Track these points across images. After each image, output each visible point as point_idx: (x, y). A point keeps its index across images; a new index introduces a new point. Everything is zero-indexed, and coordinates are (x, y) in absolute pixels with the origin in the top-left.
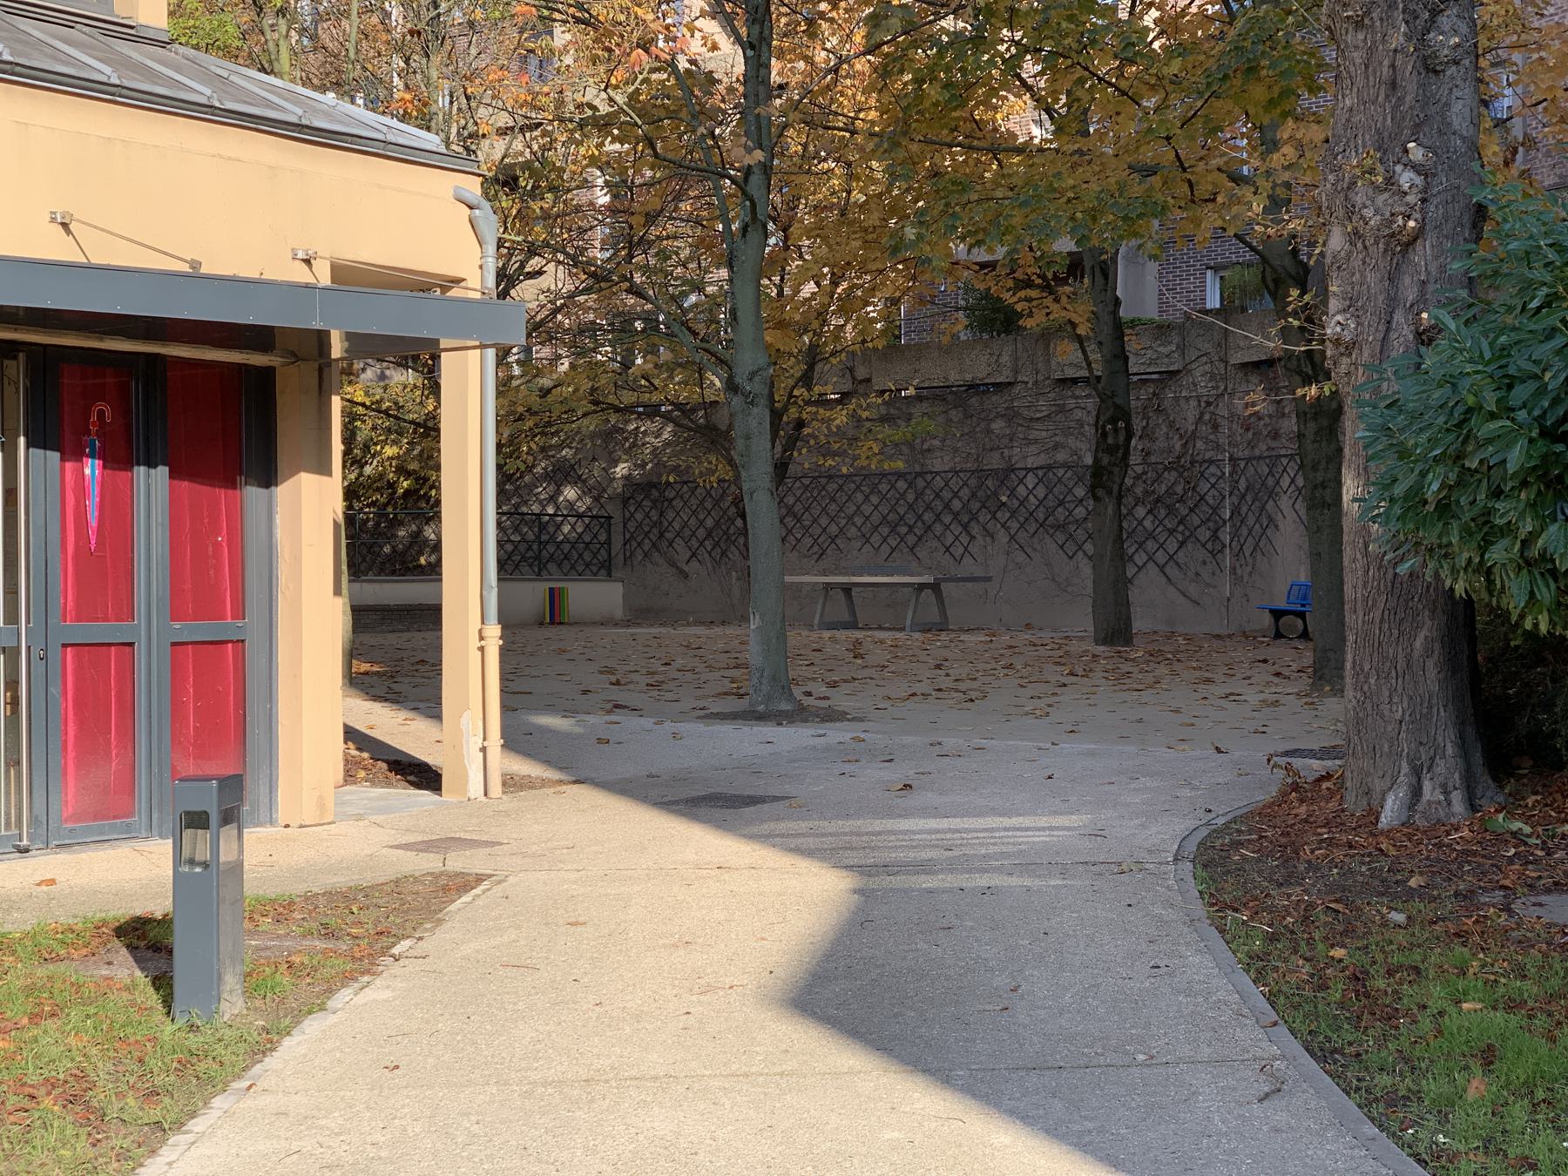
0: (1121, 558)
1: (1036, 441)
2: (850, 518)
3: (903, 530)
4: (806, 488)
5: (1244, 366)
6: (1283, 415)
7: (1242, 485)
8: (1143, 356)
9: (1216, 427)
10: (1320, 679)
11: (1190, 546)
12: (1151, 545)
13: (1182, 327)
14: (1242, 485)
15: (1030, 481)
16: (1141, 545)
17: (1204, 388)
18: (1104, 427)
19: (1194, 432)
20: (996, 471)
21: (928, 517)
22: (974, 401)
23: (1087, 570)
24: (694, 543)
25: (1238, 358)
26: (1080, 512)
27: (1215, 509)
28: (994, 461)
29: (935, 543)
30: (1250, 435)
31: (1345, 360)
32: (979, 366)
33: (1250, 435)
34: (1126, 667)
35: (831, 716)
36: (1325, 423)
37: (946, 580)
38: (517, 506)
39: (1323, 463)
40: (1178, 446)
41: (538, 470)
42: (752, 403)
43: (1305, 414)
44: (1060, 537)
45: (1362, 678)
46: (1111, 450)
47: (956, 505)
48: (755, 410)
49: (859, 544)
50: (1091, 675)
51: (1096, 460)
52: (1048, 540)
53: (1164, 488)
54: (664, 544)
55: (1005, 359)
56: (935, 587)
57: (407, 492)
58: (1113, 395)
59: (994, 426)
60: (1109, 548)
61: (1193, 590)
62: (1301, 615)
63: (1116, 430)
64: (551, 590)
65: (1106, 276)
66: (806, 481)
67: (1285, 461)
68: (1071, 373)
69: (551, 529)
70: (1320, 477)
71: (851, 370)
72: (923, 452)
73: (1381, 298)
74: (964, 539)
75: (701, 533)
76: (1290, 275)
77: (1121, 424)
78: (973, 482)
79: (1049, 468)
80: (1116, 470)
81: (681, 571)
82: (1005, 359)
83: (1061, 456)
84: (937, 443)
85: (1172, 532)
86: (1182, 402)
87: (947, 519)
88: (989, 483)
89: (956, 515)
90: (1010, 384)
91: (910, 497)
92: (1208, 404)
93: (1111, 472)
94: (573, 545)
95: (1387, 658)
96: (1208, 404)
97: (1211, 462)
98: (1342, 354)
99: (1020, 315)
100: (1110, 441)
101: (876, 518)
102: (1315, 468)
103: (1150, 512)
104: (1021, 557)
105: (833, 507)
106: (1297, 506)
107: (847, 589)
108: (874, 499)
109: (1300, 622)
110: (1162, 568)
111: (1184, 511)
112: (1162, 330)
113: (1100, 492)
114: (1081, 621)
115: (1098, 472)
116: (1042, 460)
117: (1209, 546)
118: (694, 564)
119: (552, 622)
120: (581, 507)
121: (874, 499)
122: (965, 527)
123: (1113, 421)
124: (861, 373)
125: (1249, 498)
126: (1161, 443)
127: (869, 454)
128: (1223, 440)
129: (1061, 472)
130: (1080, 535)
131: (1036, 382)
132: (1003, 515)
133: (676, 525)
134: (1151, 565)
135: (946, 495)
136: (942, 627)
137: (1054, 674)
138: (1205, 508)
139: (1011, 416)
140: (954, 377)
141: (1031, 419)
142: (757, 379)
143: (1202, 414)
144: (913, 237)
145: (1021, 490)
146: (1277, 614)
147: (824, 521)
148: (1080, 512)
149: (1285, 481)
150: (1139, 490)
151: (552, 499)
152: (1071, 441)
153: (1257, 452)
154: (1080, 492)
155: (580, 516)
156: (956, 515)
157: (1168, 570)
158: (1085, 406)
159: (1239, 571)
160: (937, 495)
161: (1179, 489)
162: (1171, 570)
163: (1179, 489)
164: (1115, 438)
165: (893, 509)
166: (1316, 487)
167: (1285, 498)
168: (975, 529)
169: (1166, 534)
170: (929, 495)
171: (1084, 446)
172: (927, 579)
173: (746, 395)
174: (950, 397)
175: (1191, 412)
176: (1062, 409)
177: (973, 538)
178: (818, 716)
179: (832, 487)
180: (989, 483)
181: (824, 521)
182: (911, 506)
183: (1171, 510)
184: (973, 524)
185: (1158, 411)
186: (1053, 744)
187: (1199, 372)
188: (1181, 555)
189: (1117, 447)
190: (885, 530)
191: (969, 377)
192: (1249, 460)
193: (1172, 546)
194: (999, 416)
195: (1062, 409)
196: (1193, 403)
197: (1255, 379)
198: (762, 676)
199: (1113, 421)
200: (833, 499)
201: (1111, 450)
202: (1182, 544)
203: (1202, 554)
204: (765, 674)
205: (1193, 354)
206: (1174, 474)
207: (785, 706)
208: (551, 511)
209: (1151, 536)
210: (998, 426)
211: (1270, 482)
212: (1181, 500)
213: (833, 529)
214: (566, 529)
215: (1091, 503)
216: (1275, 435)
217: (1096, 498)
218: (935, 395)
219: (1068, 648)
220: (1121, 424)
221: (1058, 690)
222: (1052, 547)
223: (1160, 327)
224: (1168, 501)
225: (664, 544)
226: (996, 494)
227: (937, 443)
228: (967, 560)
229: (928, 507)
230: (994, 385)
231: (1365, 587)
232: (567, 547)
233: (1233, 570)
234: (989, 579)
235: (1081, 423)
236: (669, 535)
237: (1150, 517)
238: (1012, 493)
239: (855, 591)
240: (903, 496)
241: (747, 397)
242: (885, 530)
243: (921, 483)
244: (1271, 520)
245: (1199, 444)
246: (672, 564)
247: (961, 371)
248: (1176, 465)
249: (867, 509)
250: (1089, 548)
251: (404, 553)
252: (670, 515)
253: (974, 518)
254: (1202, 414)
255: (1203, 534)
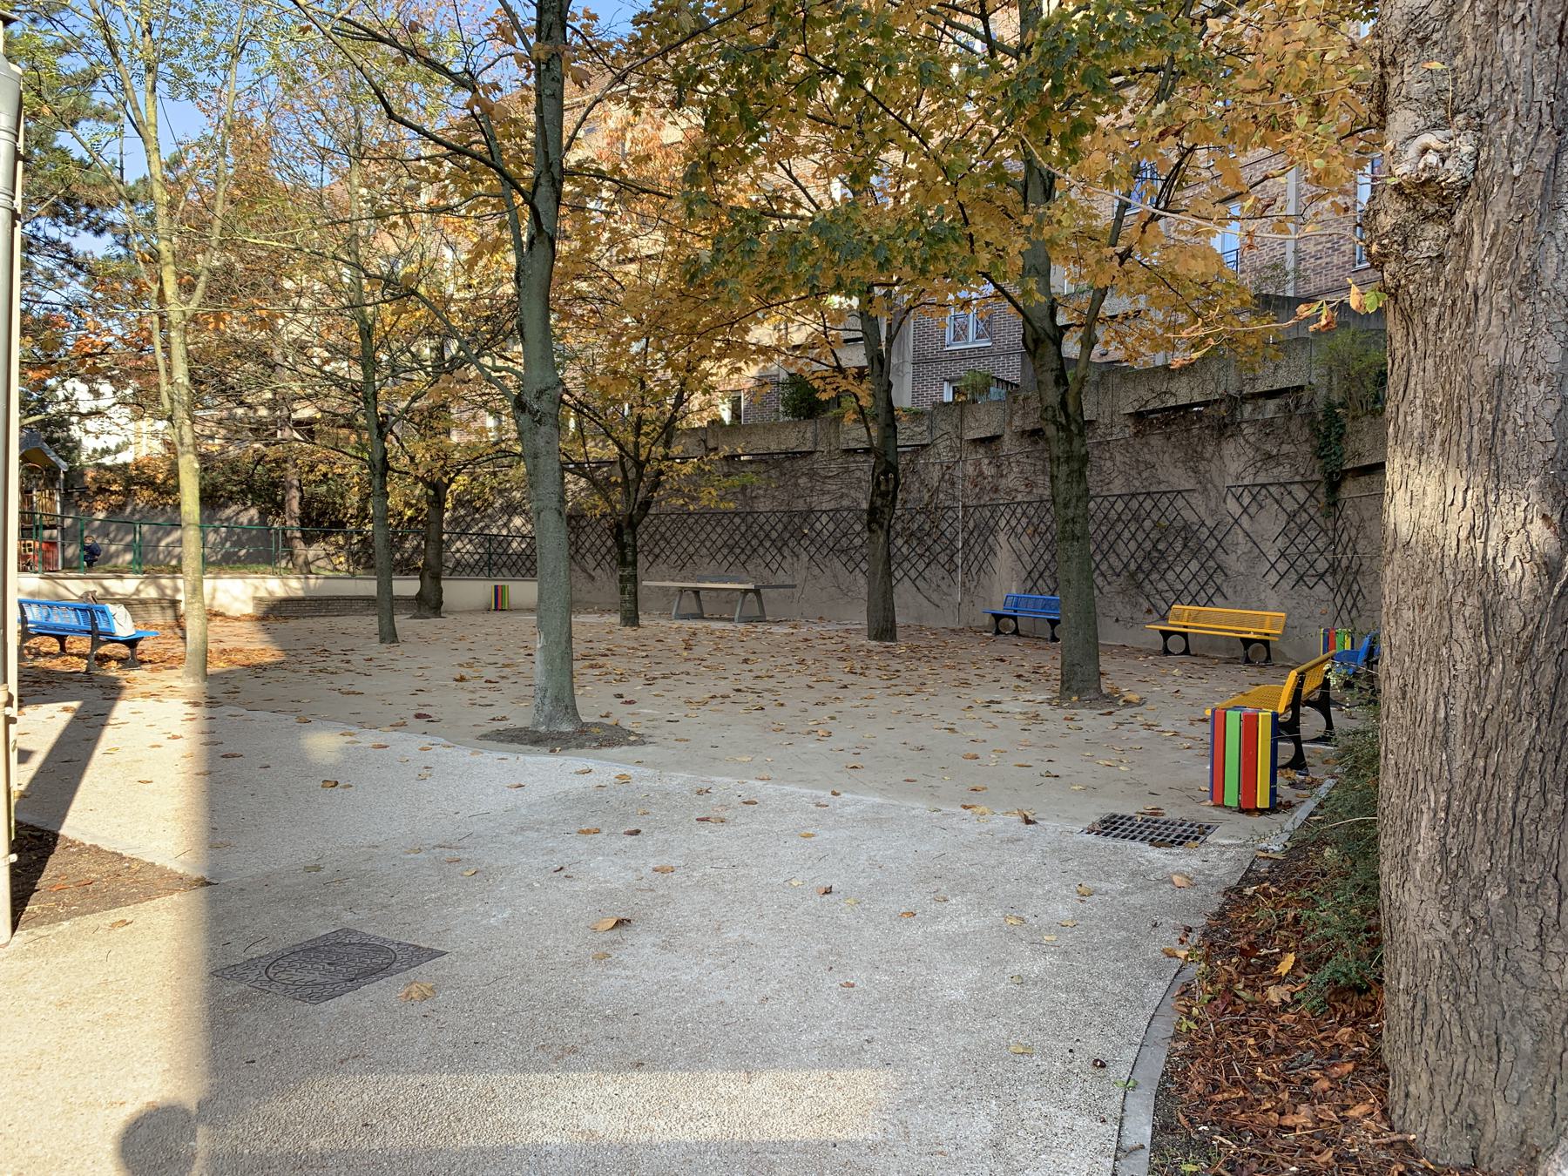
0: (889, 574)
1: (829, 492)
2: (702, 542)
3: (738, 551)
4: (673, 521)
5: (974, 441)
6: (1002, 476)
7: (971, 525)
8: (907, 434)
9: (953, 484)
10: (1068, 689)
11: (933, 566)
12: (906, 565)
13: (931, 414)
14: (971, 525)
15: (824, 519)
16: (899, 565)
17: (946, 457)
18: (878, 477)
19: (938, 487)
20: (801, 512)
21: (755, 542)
22: (787, 464)
23: (862, 581)
24: (599, 557)
25: (971, 435)
26: (858, 542)
27: (951, 542)
28: (800, 505)
29: (760, 561)
30: (977, 490)
31: (1432, 231)
32: (792, 439)
33: (977, 490)
34: (895, 664)
35: (611, 737)
36: (1076, 466)
37: (765, 587)
38: (482, 529)
39: (1074, 501)
40: (926, 497)
41: (497, 505)
42: (539, 421)
43: (1059, 458)
44: (844, 559)
45: (1464, 885)
46: (884, 495)
47: (774, 535)
48: (543, 429)
49: (708, 560)
50: (867, 672)
51: (872, 503)
52: (836, 560)
53: (916, 526)
54: (579, 557)
55: (808, 435)
56: (757, 591)
57: (411, 519)
58: (885, 454)
59: (800, 481)
60: (880, 567)
61: (935, 597)
62: (1015, 618)
63: (887, 480)
64: (496, 587)
65: (882, 365)
66: (674, 517)
67: (1002, 508)
68: (853, 445)
69: (505, 545)
70: (1070, 513)
71: (705, 441)
72: (752, 498)
73: (1541, 82)
74: (779, 558)
75: (604, 550)
76: (1049, 337)
77: (891, 476)
78: (785, 519)
79: (837, 510)
80: (886, 510)
81: (590, 576)
82: (808, 435)
83: (845, 503)
84: (761, 492)
85: (921, 556)
86: (930, 466)
87: (767, 544)
88: (796, 520)
89: (773, 541)
90: (811, 453)
91: (743, 529)
92: (948, 468)
93: (883, 512)
94: (519, 556)
95: (1533, 852)
96: (948, 468)
97: (949, 508)
98: (1427, 218)
99: (817, 391)
100: (883, 488)
101: (719, 543)
102: (1066, 506)
103: (906, 542)
104: (817, 571)
105: (691, 534)
106: (1011, 540)
107: (696, 592)
108: (719, 530)
109: (1011, 622)
110: (914, 582)
111: (930, 542)
112: (917, 416)
113: (874, 526)
114: (858, 618)
115: (872, 511)
116: (832, 505)
117: (947, 566)
118: (599, 571)
119: (496, 609)
120: (525, 531)
121: (719, 530)
122: (780, 550)
123: (885, 473)
124: (711, 444)
125: (975, 534)
126: (915, 495)
127: (709, 497)
128: (958, 493)
129: (845, 514)
130: (858, 557)
131: (829, 452)
132: (804, 542)
133: (587, 544)
134: (906, 578)
135: (767, 528)
136: (761, 619)
137: (838, 671)
138: (944, 540)
139: (812, 475)
140: (774, 447)
141: (826, 477)
142: (545, 397)
143: (943, 475)
144: (708, 261)
145: (818, 526)
146: (998, 617)
147: (685, 544)
148: (858, 542)
149: (1003, 523)
150: (898, 527)
151: (506, 525)
152: (852, 492)
153: (982, 502)
154: (858, 527)
155: (524, 537)
156: (773, 541)
157: (917, 582)
158: (864, 468)
159: (967, 584)
160: (761, 528)
161: (927, 527)
162: (920, 583)
163: (927, 527)
164: (887, 485)
165: (731, 536)
166: (1067, 522)
167: (1002, 534)
168: (786, 552)
169: (916, 558)
170: (756, 528)
171: (861, 496)
172: (751, 586)
173: (534, 413)
174: (771, 462)
175: (936, 473)
176: (847, 470)
177: (784, 557)
178: (596, 740)
179: (690, 521)
180: (796, 520)
181: (685, 544)
182: (743, 535)
183: (920, 541)
184: (785, 548)
185: (914, 472)
186: (834, 794)
187: (942, 445)
188: (927, 574)
189: (888, 493)
190: (725, 551)
191: (783, 447)
192: (976, 507)
193: (921, 566)
194: (803, 474)
195: (847, 470)
196: (938, 467)
197: (982, 451)
198: (544, 697)
199: (885, 473)
200: (691, 529)
201: (884, 495)
202: (928, 565)
203: (942, 572)
204: (548, 694)
205: (938, 433)
206: (923, 516)
207: (566, 728)
208: (504, 532)
209: (906, 558)
210: (802, 481)
211: (992, 523)
212: (928, 534)
213: (691, 549)
214: (514, 545)
215: (866, 535)
216: (996, 490)
217: (871, 531)
218: (764, 460)
219: (848, 642)
220: (891, 476)
221: (841, 693)
222: (838, 565)
223: (916, 413)
224: (919, 535)
225: (579, 557)
226: (800, 528)
227: (761, 492)
228: (780, 572)
229: (755, 536)
230: (800, 453)
231: (1479, 695)
232: (515, 557)
233: (963, 583)
234: (794, 586)
235: (859, 480)
236: (582, 551)
237: (906, 546)
238: (812, 528)
239: (702, 593)
240: (738, 528)
241: (535, 415)
242: (725, 551)
243: (750, 520)
244: (991, 549)
245: (941, 495)
246: (584, 571)
247: (779, 443)
248: (924, 510)
249: (714, 536)
250: (864, 566)
251: (408, 560)
252: (583, 537)
253: (786, 544)
254: (943, 475)
255: (943, 558)
